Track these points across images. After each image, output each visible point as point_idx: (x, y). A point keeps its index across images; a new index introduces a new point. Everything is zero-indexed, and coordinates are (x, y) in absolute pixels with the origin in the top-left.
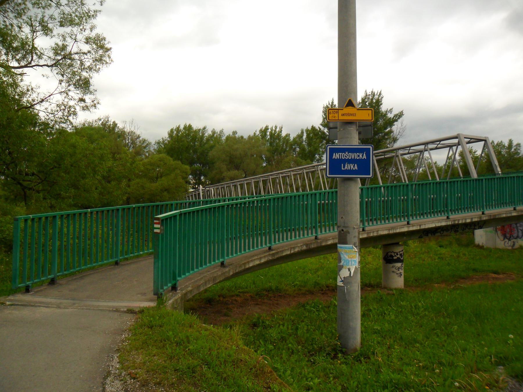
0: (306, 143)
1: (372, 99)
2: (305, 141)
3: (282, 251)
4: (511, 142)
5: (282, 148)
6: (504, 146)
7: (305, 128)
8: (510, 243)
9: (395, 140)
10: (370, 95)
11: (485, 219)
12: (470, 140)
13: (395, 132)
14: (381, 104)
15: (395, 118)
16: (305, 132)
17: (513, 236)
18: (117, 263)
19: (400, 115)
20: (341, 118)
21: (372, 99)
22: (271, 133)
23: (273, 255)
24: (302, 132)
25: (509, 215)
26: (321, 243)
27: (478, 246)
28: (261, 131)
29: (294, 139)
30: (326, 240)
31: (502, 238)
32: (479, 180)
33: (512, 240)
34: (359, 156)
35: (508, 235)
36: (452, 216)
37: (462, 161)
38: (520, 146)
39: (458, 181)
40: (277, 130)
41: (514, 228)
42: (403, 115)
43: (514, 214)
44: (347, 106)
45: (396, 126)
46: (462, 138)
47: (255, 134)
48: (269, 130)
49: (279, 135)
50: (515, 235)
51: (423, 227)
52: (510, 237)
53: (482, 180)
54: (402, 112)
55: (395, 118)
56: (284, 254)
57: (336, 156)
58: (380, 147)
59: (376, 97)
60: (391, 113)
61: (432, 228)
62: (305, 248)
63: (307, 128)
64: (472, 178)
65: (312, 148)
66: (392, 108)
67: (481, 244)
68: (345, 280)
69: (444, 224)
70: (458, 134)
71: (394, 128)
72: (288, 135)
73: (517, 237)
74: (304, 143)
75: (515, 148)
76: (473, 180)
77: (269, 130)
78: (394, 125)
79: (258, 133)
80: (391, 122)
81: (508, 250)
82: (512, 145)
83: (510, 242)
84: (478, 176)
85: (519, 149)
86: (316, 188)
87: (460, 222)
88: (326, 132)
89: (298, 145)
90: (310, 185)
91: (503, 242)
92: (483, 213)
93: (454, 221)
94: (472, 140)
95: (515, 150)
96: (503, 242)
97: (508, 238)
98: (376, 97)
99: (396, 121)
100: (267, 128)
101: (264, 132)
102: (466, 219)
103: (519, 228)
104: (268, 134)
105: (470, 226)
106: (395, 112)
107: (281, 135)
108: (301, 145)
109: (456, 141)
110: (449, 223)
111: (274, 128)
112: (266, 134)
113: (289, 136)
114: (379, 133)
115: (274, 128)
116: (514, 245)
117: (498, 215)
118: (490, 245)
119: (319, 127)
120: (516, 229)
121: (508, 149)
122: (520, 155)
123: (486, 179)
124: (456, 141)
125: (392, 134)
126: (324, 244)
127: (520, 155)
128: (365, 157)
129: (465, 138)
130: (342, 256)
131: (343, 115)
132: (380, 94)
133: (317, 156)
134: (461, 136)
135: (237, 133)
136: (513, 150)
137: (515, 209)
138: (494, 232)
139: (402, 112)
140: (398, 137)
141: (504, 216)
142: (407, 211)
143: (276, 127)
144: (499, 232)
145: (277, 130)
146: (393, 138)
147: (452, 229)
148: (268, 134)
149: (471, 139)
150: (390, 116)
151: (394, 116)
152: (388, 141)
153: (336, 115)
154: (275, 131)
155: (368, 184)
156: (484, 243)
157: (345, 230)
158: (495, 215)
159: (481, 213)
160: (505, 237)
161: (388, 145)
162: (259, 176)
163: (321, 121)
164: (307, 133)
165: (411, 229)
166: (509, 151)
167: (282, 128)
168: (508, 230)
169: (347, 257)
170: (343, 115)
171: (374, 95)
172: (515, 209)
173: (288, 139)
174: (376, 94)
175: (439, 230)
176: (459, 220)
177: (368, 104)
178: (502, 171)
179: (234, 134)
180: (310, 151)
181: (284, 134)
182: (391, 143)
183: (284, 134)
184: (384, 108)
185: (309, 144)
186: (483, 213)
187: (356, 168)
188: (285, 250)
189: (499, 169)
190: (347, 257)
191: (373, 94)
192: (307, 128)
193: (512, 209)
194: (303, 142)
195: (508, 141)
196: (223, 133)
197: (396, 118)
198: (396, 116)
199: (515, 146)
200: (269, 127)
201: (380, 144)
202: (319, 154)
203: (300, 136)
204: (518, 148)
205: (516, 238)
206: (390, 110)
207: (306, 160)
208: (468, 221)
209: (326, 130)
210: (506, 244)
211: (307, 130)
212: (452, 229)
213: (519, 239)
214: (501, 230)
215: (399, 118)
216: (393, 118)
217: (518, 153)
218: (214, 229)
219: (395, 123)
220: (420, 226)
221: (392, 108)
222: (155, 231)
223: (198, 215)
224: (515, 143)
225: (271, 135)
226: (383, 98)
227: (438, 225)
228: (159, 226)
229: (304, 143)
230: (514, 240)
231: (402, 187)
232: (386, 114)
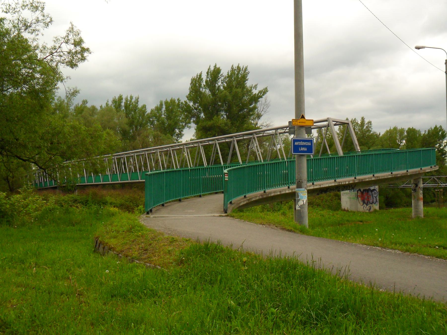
0: (165, 116)
1: (238, 74)
2: (164, 114)
3: (240, 203)
4: (363, 119)
5: (138, 121)
6: (357, 123)
7: (164, 100)
8: (368, 207)
9: (259, 116)
10: (235, 69)
11: (356, 182)
12: (336, 123)
13: (259, 108)
14: (247, 80)
15: (259, 94)
16: (164, 104)
17: (369, 202)
18: (163, 205)
19: (264, 92)
20: (299, 124)
21: (238, 74)
22: (126, 103)
23: (248, 200)
24: (161, 105)
25: (370, 180)
26: (268, 194)
27: (345, 210)
28: (114, 101)
29: (152, 111)
30: (270, 193)
31: (362, 203)
32: (344, 157)
33: (369, 205)
34: (307, 144)
35: (366, 201)
36: (338, 180)
37: (320, 137)
38: (371, 124)
39: (323, 159)
40: (133, 100)
41: (370, 195)
42: (267, 91)
43: (373, 179)
44: (301, 118)
45: (260, 102)
46: (331, 121)
47: (107, 104)
48: (124, 101)
49: (136, 107)
50: (371, 201)
51: (322, 186)
52: (368, 203)
53: (334, 158)
54: (266, 88)
55: (259, 94)
56: (241, 204)
57: (296, 143)
58: (245, 123)
59: (242, 72)
60: (256, 89)
61: (325, 187)
62: (261, 197)
63: (166, 100)
64: (339, 156)
65: (170, 122)
66: (257, 85)
67: (346, 209)
68: (301, 207)
69: (333, 184)
70: (328, 118)
71: (258, 105)
72: (144, 106)
73: (373, 202)
74: (163, 116)
75: (367, 125)
76: (340, 157)
77: (124, 101)
78: (259, 102)
79: (110, 103)
80: (256, 99)
81: (366, 212)
82: (364, 123)
83: (367, 206)
84: (344, 153)
85: (370, 127)
86: (168, 168)
87: (343, 184)
88: (191, 105)
89: (156, 117)
90: (163, 165)
91: (363, 206)
92: (355, 178)
93: (339, 182)
94: (338, 123)
95: (367, 127)
96: (363, 206)
97: (366, 203)
98: (242, 72)
99: (261, 97)
100: (121, 98)
101: (117, 102)
102: (346, 182)
103: (374, 195)
104: (123, 104)
105: (347, 187)
106: (260, 88)
107: (137, 106)
108: (160, 118)
109: (326, 123)
110: (336, 184)
111: (129, 98)
112: (120, 105)
113: (145, 108)
114: (244, 109)
115: (129, 98)
116: (370, 209)
117: (364, 179)
118: (353, 209)
119: (185, 101)
120: (371, 196)
121: (361, 127)
122: (371, 133)
123: (356, 156)
124: (326, 123)
125: (257, 110)
126: (269, 196)
127: (371, 133)
128: (310, 144)
129: (333, 121)
130: (299, 194)
131: (299, 122)
132: (246, 69)
133: (177, 131)
134: (330, 119)
135: (87, 103)
136: (365, 128)
137: (373, 176)
138: (356, 198)
139: (266, 88)
140: (262, 113)
141: (368, 180)
142: (313, 178)
143: (131, 98)
144: (360, 199)
145: (133, 100)
146: (258, 114)
147: (336, 189)
148: (123, 104)
149: (337, 122)
150: (255, 92)
151: (259, 93)
152: (252, 117)
153: (296, 123)
154: (131, 101)
155: (212, 164)
156: (349, 207)
157: (300, 181)
158: (362, 180)
159: (354, 178)
160: (364, 202)
161: (252, 122)
162: (133, 151)
163: (188, 92)
164: (166, 106)
165: (315, 187)
166: (362, 129)
167: (138, 98)
168: (366, 197)
169: (302, 195)
170: (299, 122)
171: (240, 70)
172: (373, 176)
173: (144, 111)
174: (241, 69)
175: (329, 190)
176: (342, 182)
177: (233, 79)
178: (361, 149)
179: (84, 103)
180: (169, 125)
181: (140, 105)
182: (255, 119)
183: (140, 105)
184: (249, 84)
185: (169, 118)
186: (355, 178)
187: (306, 150)
188: (242, 202)
189: (359, 148)
190: (302, 195)
191: (238, 67)
192: (166, 100)
193: (372, 176)
194: (162, 115)
195: (361, 119)
196: (71, 102)
197: (261, 94)
198: (260, 92)
199: (367, 124)
200: (124, 97)
201: (245, 119)
202: (179, 129)
203: (159, 109)
204: (370, 126)
205: (371, 204)
206: (255, 86)
207: (166, 134)
208: (347, 183)
209: (191, 104)
210: (365, 208)
211: (166, 103)
212: (336, 189)
213: (373, 204)
214: (361, 197)
215: (263, 95)
216: (258, 94)
217: (369, 131)
218: (194, 190)
219: (260, 99)
220: (320, 185)
221: (257, 85)
222: (226, 179)
223: (332, 160)
224: (366, 121)
225: (126, 107)
226: (249, 74)
227: (330, 185)
228: (227, 177)
229: (163, 116)
230: (370, 205)
231: (324, 159)
232: (250, 91)
